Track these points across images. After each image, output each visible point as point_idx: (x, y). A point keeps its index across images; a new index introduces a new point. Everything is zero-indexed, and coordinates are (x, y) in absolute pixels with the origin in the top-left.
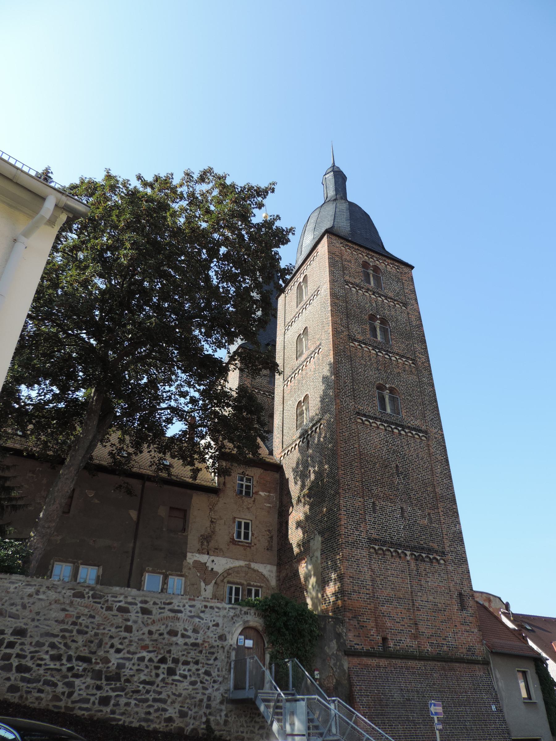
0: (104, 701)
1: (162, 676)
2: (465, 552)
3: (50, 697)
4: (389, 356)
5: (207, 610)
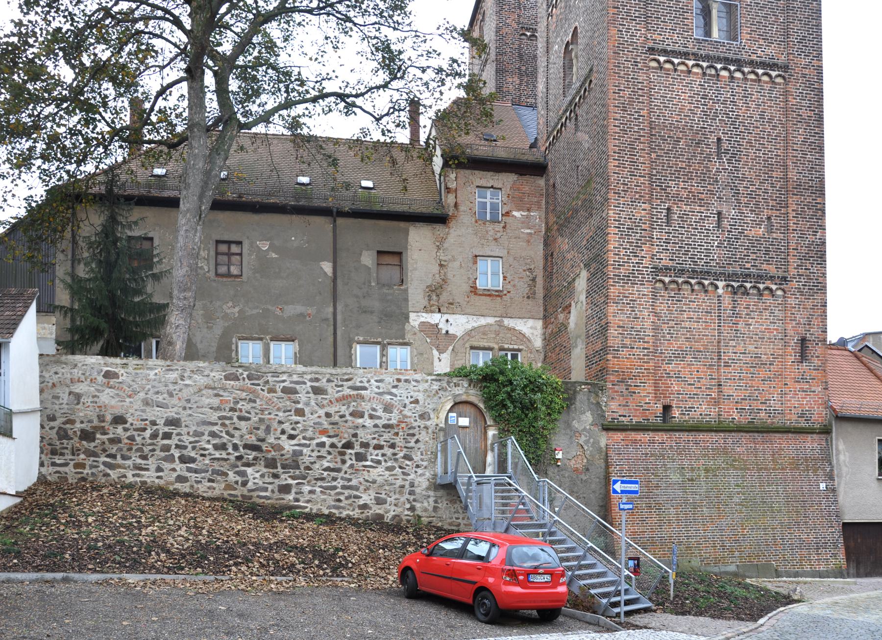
1: (349, 463)
2: (824, 274)
3: (223, 486)
5: (400, 384)
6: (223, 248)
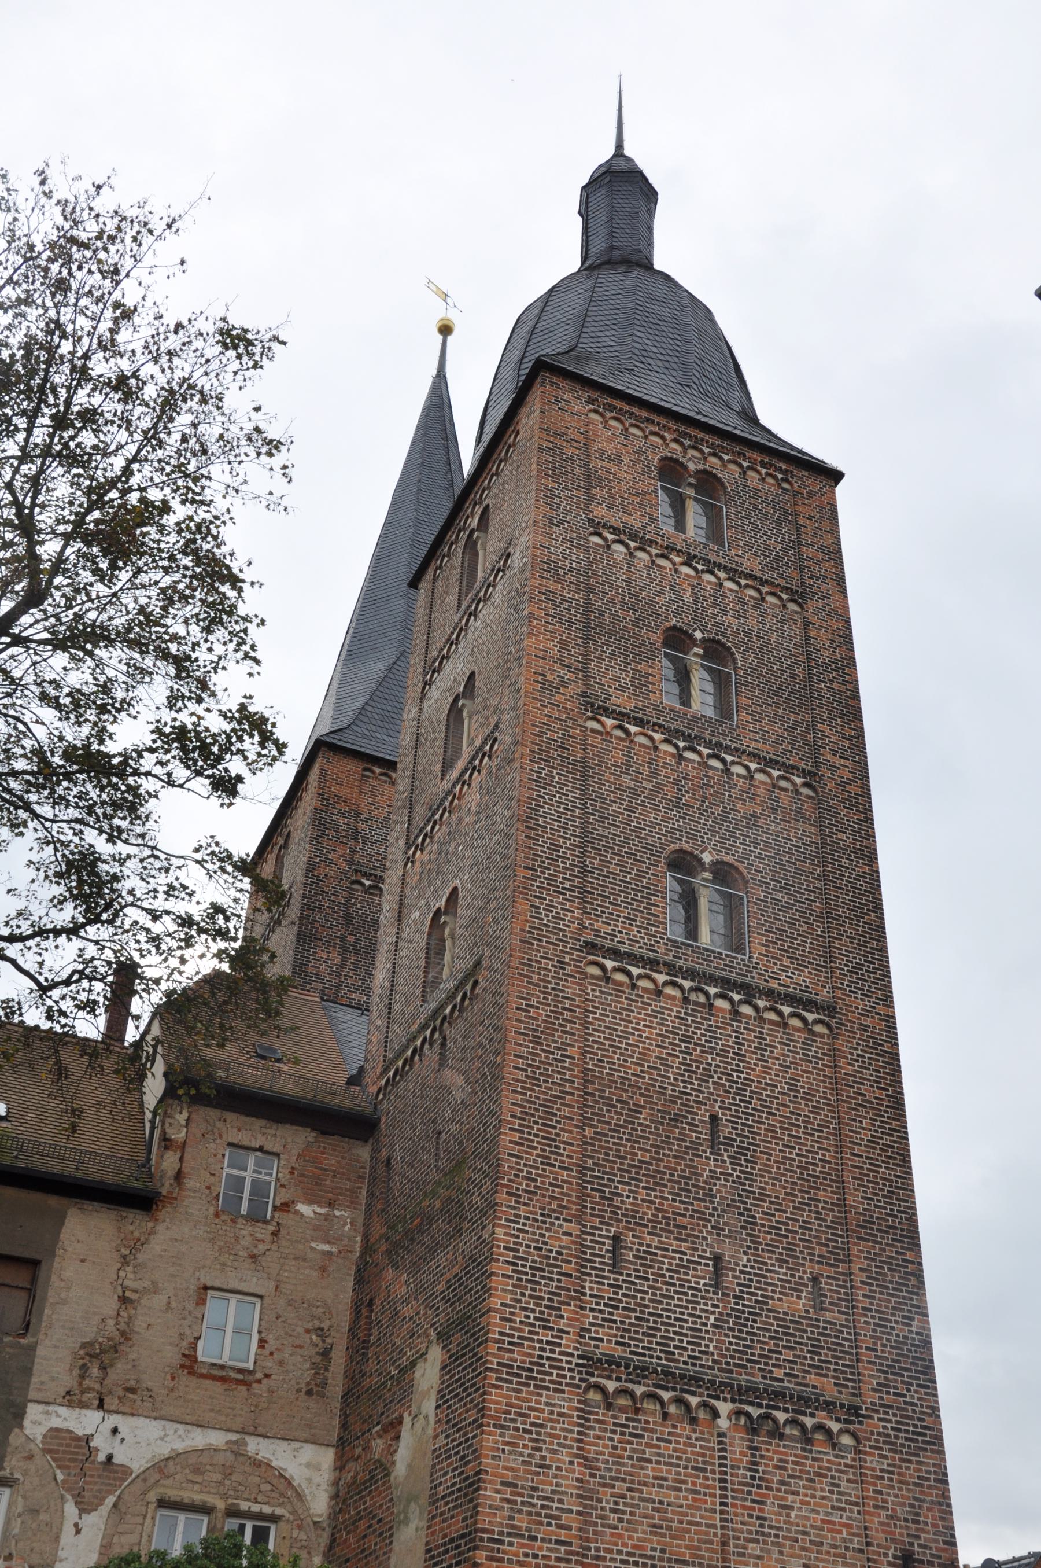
4: (723, 761)
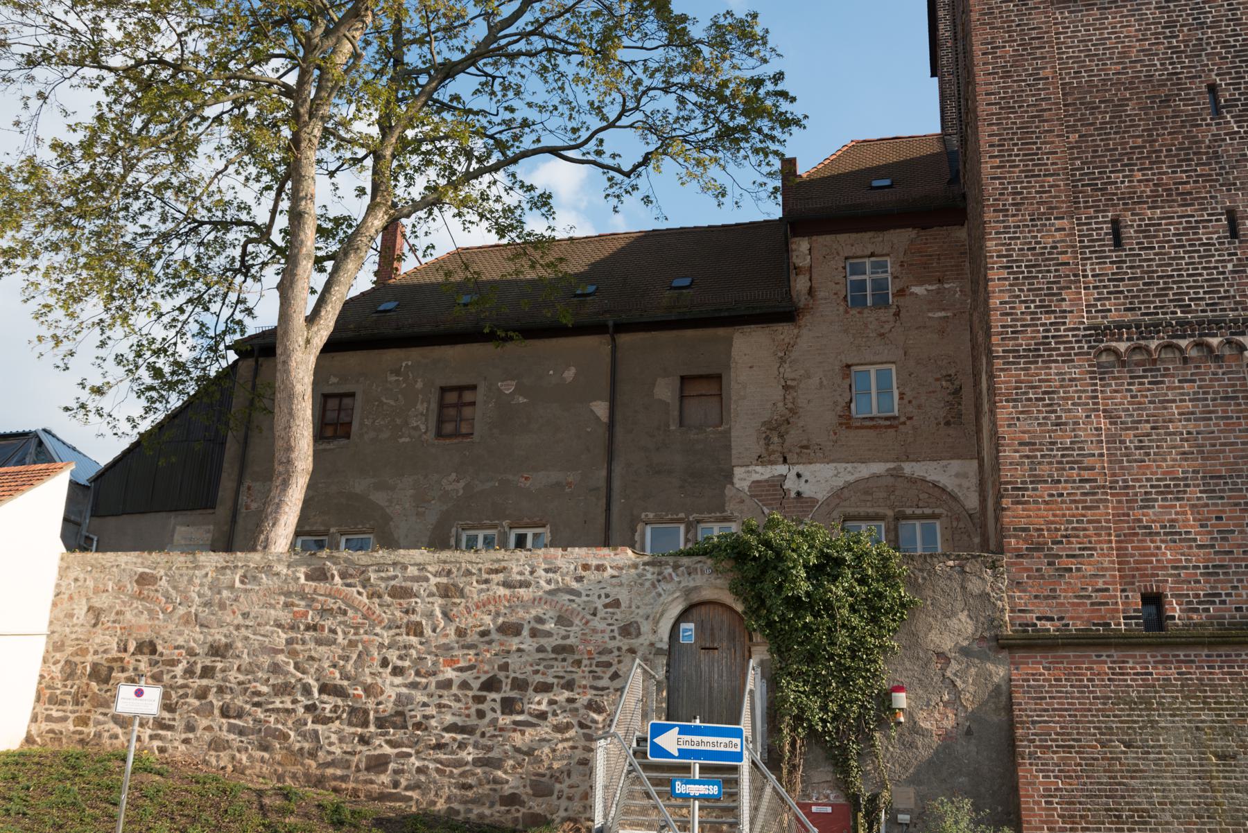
0: (378, 764)
1: (490, 716)
6: (452, 397)
